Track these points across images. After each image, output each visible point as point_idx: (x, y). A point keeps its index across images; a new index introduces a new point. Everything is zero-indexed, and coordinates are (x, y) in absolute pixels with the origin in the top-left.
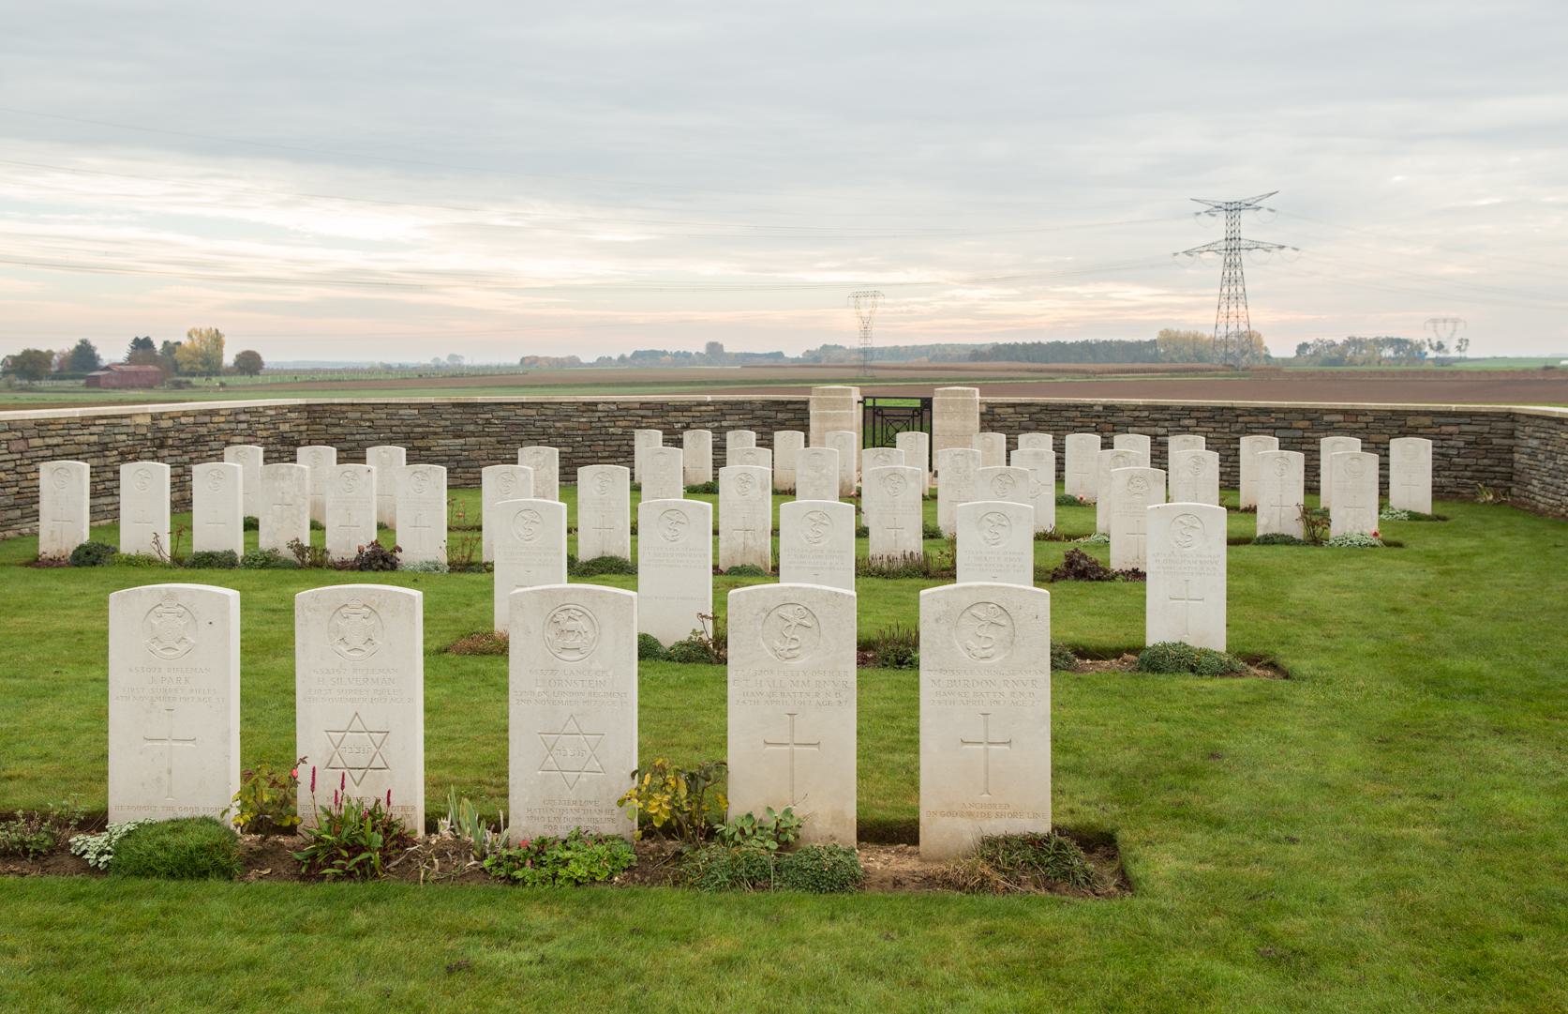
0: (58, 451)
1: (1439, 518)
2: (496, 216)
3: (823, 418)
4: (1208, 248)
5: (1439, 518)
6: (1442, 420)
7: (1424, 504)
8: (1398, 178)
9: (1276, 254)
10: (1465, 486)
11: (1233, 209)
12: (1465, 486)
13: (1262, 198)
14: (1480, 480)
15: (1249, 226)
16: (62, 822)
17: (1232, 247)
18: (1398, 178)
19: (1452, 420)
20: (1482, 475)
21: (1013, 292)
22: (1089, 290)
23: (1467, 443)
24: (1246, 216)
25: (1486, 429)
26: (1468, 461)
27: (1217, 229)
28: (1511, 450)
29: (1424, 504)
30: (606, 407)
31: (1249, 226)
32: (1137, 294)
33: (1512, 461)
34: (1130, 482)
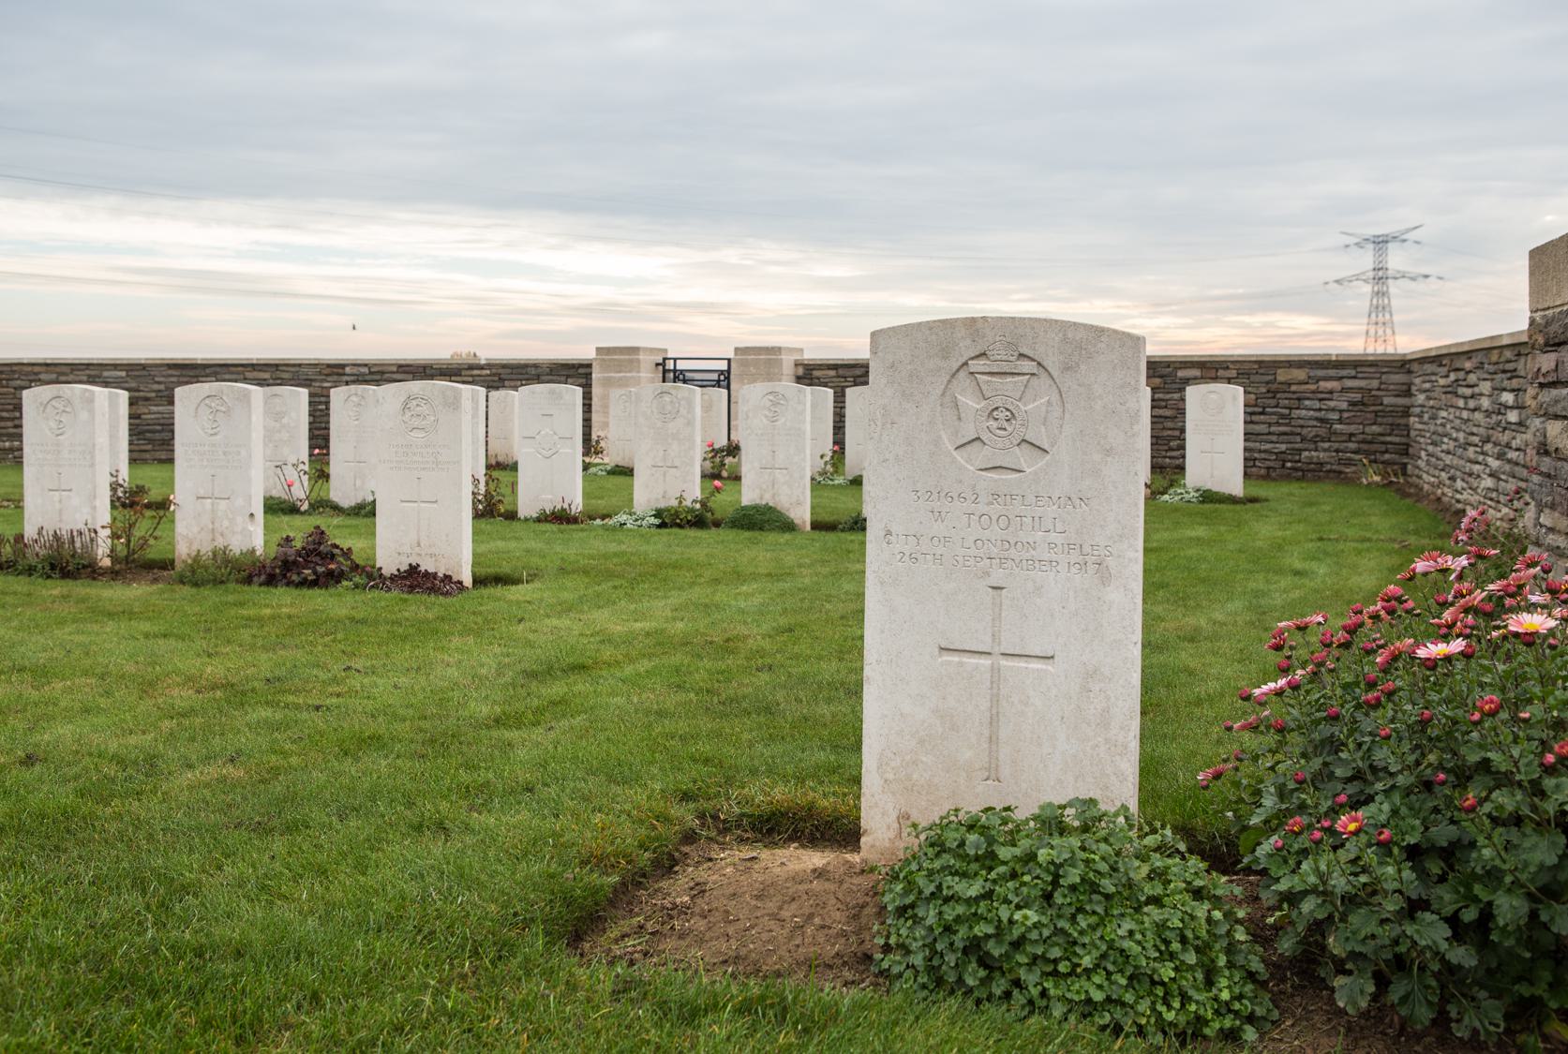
0: (147, 456)
1: (1253, 500)
2: (731, 255)
3: (608, 383)
4: (1357, 278)
5: (1253, 500)
6: (1320, 373)
7: (1233, 483)
8: (1549, 218)
9: (1420, 286)
10: (1349, 463)
11: (1381, 242)
12: (1349, 463)
13: (1408, 231)
14: (1367, 453)
15: (1396, 259)
17: (1380, 277)
18: (1549, 218)
19: (1332, 372)
20: (1371, 449)
21: (1188, 321)
23: (1352, 404)
25: (1375, 384)
26: (1352, 429)
27: (1366, 260)
28: (1406, 412)
29: (1233, 483)
30: (355, 370)
31: (1396, 259)
32: (1305, 323)
34: (405, 407)
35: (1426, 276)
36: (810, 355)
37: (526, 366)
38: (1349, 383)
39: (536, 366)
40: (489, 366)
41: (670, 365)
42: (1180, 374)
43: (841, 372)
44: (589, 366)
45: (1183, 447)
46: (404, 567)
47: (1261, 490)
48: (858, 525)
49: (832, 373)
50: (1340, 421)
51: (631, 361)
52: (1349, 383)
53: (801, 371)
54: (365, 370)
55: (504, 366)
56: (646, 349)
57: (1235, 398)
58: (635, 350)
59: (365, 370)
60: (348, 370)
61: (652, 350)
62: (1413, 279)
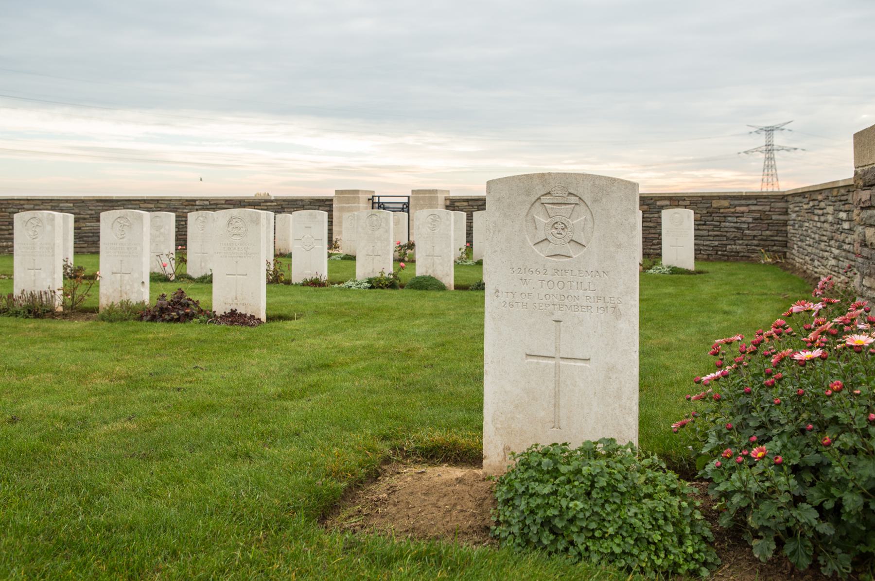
0: (84, 250)
1: (700, 272)
2: (410, 140)
3: (342, 209)
5: (700, 272)
6: (737, 202)
7: (688, 262)
8: (864, 116)
9: (792, 154)
10: (754, 251)
11: (770, 131)
12: (754, 251)
14: (764, 246)
15: (778, 140)
16: (594, 443)
17: (769, 149)
18: (864, 116)
19: (743, 202)
20: (766, 244)
22: (700, 173)
23: (755, 219)
24: (776, 133)
25: (768, 208)
26: (755, 233)
27: (761, 141)
28: (785, 224)
29: (688, 262)
30: (201, 203)
31: (778, 140)
33: (786, 232)
35: (796, 149)
36: (453, 194)
37: (296, 200)
38: (753, 208)
39: (302, 200)
40: (276, 200)
41: (376, 200)
42: (658, 203)
43: (470, 203)
44: (331, 200)
45: (660, 244)
46: (228, 311)
47: (704, 267)
48: (481, 287)
49: (466, 204)
50: (748, 229)
51: (355, 198)
52: (753, 208)
53: (448, 203)
54: (207, 203)
55: (284, 201)
56: (363, 191)
57: (689, 217)
58: (357, 192)
59: (207, 203)
60: (197, 203)
61: (366, 192)
62: (788, 150)
